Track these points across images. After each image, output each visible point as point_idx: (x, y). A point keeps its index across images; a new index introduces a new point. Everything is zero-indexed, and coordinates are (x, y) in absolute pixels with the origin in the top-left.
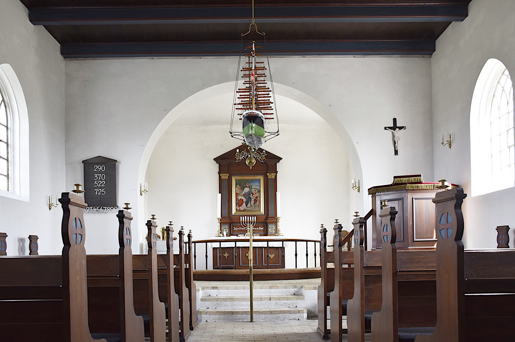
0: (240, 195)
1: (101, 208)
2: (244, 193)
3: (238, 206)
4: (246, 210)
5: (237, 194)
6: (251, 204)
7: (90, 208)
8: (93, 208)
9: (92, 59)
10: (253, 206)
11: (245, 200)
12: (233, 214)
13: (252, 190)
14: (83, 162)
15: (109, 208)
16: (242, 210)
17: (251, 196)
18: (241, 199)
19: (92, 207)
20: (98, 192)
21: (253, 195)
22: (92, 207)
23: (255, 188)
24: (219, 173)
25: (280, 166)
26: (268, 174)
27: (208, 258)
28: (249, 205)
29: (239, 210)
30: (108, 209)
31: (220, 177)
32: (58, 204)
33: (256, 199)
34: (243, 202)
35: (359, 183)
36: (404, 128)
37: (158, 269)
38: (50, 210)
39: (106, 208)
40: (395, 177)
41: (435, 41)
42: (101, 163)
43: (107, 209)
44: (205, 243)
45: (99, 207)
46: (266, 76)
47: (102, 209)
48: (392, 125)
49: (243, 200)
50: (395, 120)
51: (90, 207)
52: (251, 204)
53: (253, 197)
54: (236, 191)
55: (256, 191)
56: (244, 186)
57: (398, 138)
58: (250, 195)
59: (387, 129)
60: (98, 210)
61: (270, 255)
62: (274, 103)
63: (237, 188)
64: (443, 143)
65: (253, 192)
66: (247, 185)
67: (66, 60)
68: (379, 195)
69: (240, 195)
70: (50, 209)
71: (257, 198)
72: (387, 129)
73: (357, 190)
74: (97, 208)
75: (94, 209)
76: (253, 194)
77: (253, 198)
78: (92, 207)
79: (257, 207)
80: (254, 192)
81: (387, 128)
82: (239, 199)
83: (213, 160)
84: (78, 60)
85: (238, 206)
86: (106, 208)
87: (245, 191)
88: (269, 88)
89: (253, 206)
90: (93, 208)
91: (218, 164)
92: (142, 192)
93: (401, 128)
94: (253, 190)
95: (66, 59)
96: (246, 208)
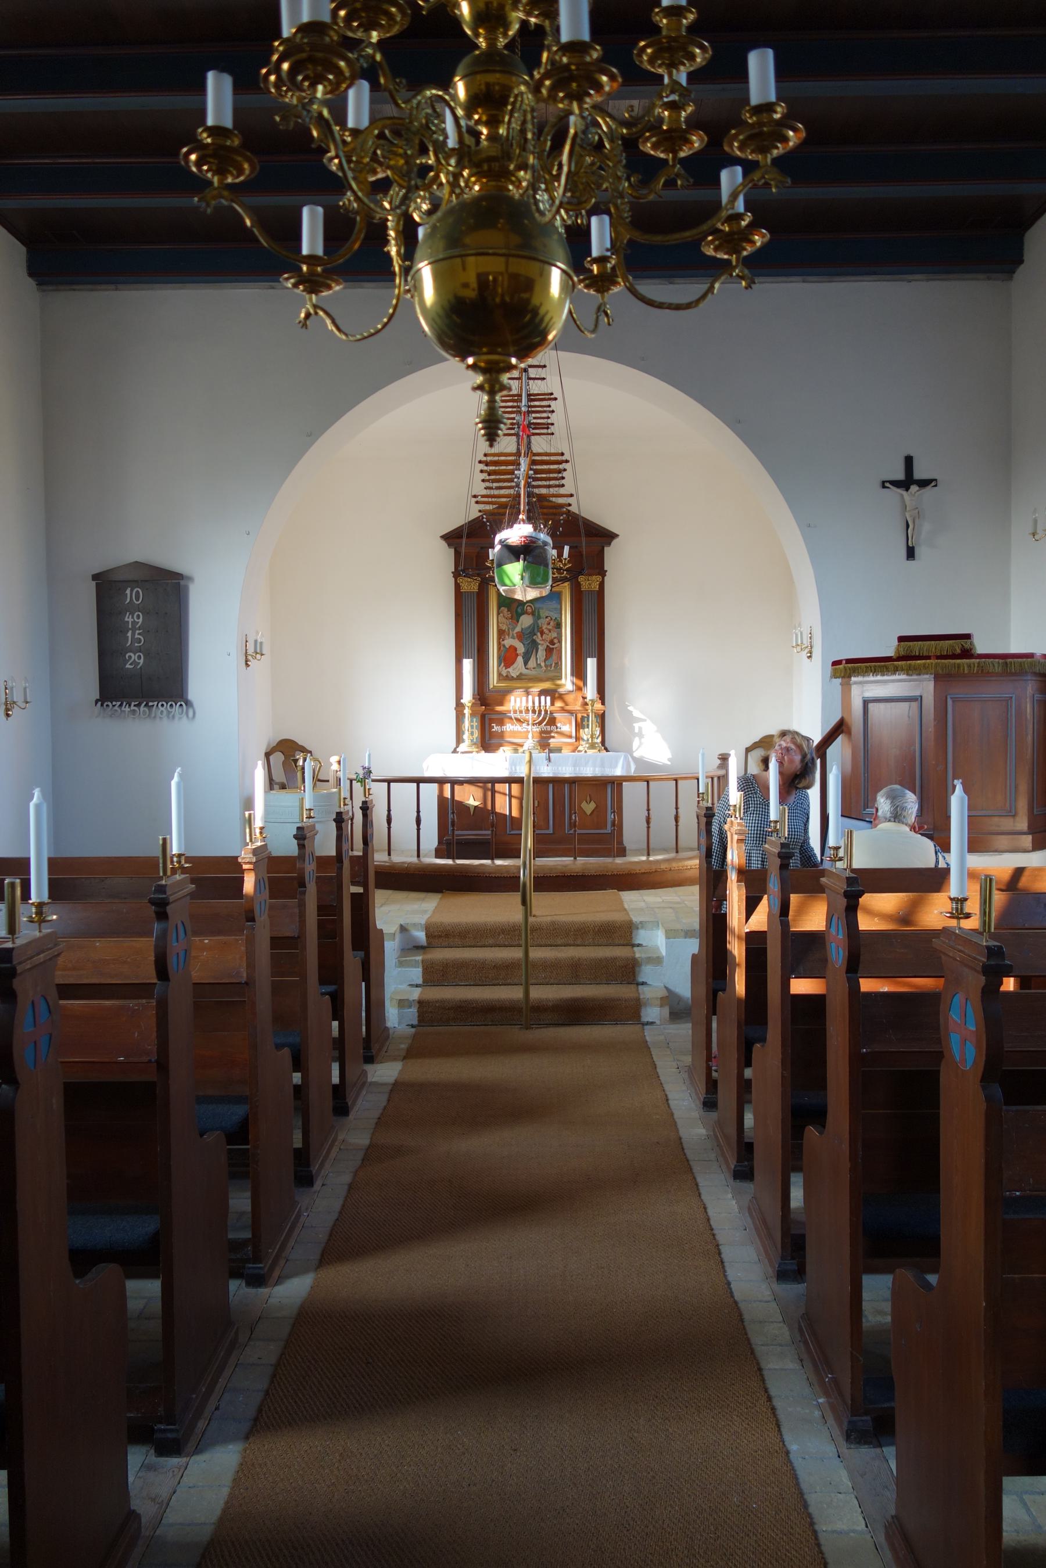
0: (509, 635)
1: (143, 705)
2: (518, 629)
3: (503, 664)
4: (523, 677)
5: (501, 633)
6: (537, 659)
7: (114, 706)
8: (121, 705)
9: (113, 287)
10: (543, 664)
11: (521, 648)
12: (491, 686)
13: (540, 622)
14: (95, 577)
15: (162, 705)
16: (515, 677)
17: (538, 638)
18: (511, 646)
19: (120, 703)
20: (134, 661)
21: (542, 636)
22: (119, 703)
23: (546, 617)
24: (456, 574)
25: (612, 556)
26: (581, 579)
27: (421, 827)
28: (532, 663)
29: (507, 676)
30: (161, 708)
31: (457, 586)
32: (28, 700)
33: (551, 646)
34: (517, 655)
35: (811, 634)
36: (933, 484)
37: (230, 1151)
38: (9, 718)
39: (155, 706)
40: (901, 639)
41: (1023, 235)
42: (142, 581)
43: (159, 709)
44: (415, 784)
45: (136, 703)
46: (553, 434)
47: (145, 705)
48: (900, 476)
49: (516, 649)
50: (909, 461)
51: (114, 703)
52: (537, 659)
53: (543, 640)
54: (500, 625)
55: (552, 623)
56: (519, 610)
57: (917, 511)
58: (535, 635)
59: (888, 488)
60: (134, 710)
61: (584, 805)
62: (575, 496)
63: (501, 615)
64: (1034, 535)
65: (541, 628)
66: (529, 608)
67: (44, 291)
68: (860, 683)
69: (509, 635)
70: (8, 715)
71: (552, 642)
72: (888, 488)
73: (805, 654)
74: (133, 704)
75: (123, 708)
76: (542, 633)
77: (542, 645)
78: (119, 703)
79: (553, 668)
80: (546, 628)
81: (887, 485)
82: (507, 647)
83: (439, 538)
84: (74, 290)
85: (503, 664)
86: (155, 706)
87: (522, 624)
88: (562, 454)
89: (543, 664)
90: (121, 705)
91: (453, 550)
92: (250, 657)
93: (924, 483)
94: (543, 623)
95: (45, 287)
96: (525, 671)
